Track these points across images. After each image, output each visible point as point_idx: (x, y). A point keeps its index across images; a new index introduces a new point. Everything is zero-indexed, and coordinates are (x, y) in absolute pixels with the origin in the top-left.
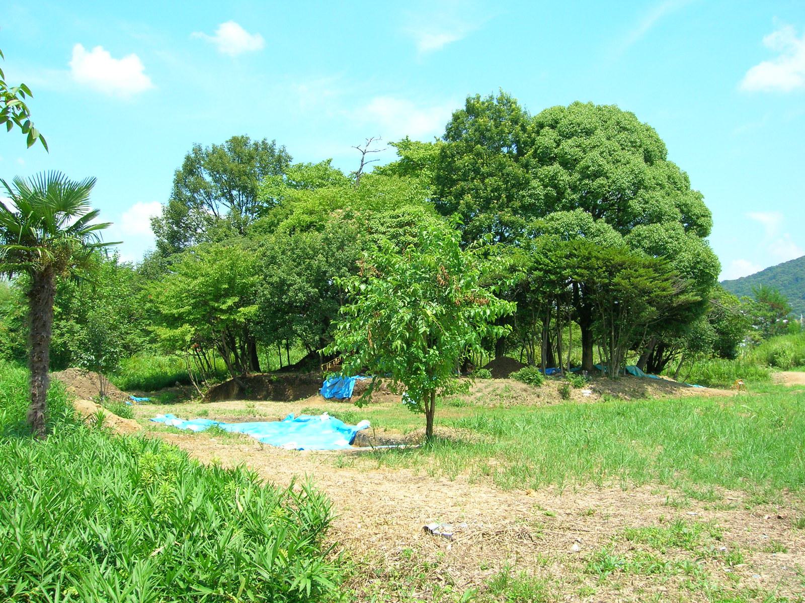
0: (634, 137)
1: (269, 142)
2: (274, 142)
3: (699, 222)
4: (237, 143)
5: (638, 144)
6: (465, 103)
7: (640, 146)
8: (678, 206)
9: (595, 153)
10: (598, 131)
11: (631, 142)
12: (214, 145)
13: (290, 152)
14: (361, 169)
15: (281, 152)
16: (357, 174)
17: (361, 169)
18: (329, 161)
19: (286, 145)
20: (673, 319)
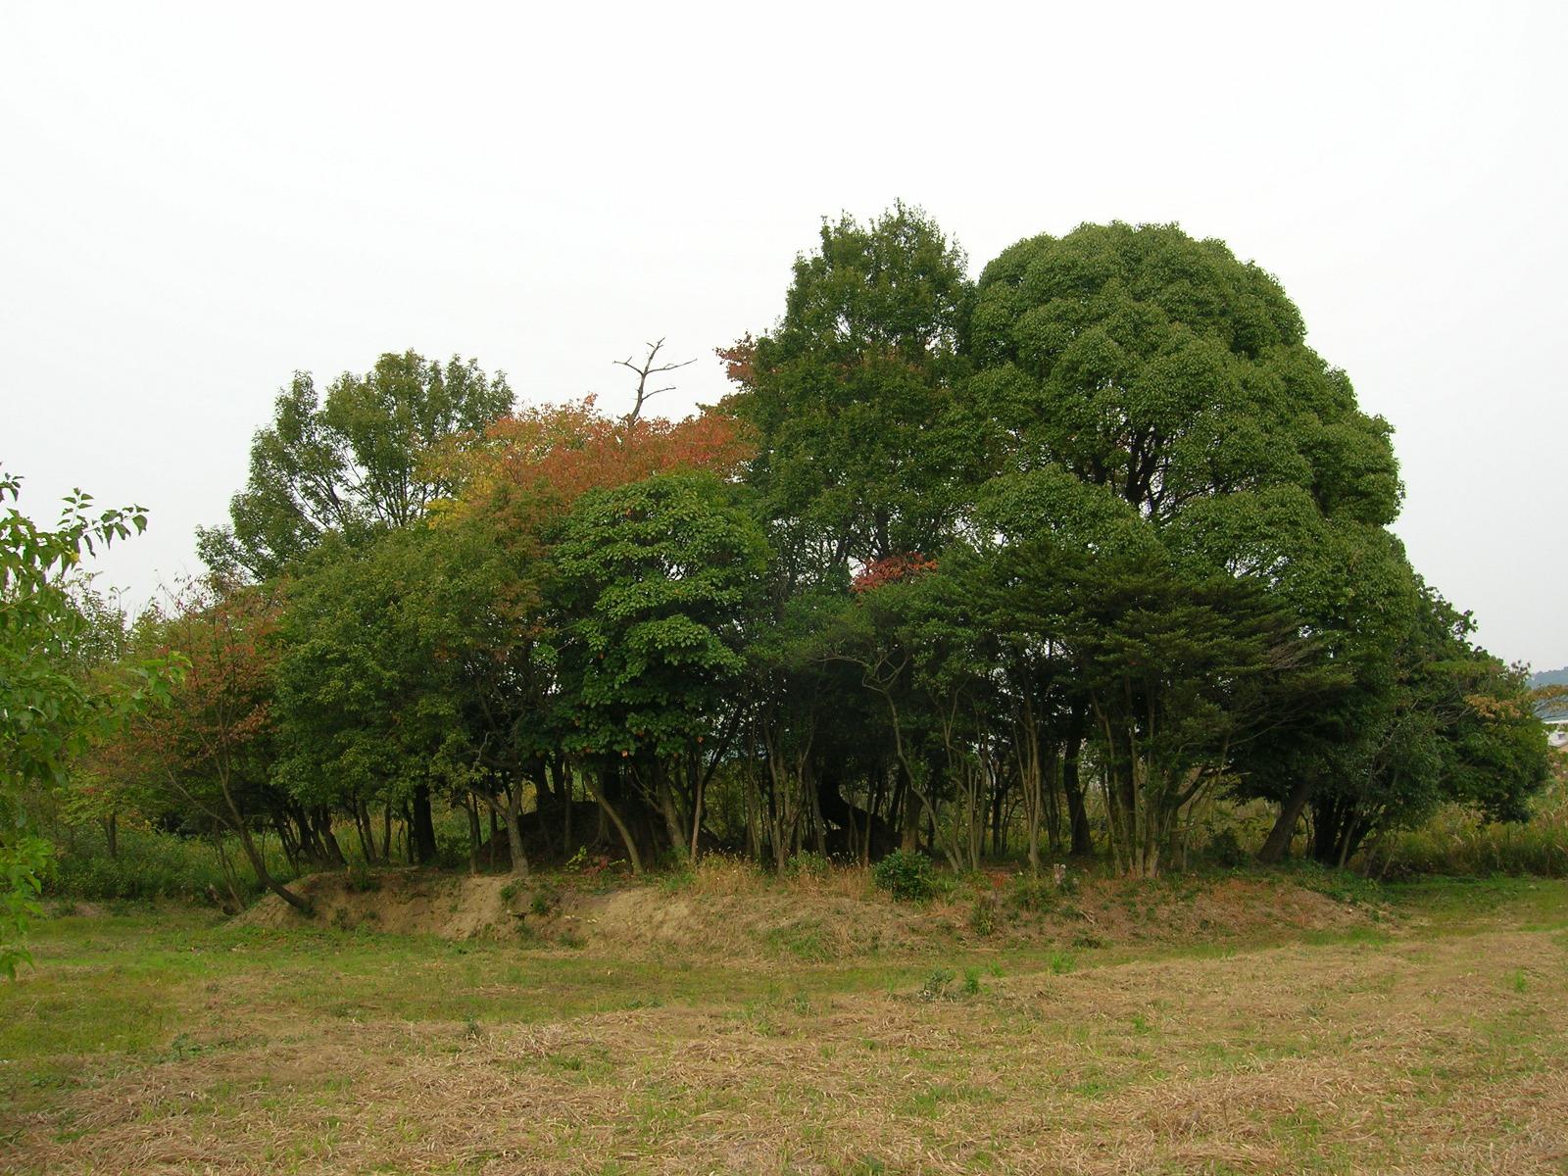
0: (1206, 292)
1: (464, 363)
2: (473, 362)
3: (1363, 484)
4: (398, 369)
5: (1216, 307)
6: (820, 242)
7: (1223, 313)
8: (1305, 449)
9: (1098, 331)
10: (1114, 283)
11: (1197, 303)
12: (1451, 604)
13: (513, 384)
14: (637, 411)
15: (495, 385)
16: (630, 418)
17: (637, 411)
18: (590, 400)
19: (504, 371)
20: (1084, 918)
